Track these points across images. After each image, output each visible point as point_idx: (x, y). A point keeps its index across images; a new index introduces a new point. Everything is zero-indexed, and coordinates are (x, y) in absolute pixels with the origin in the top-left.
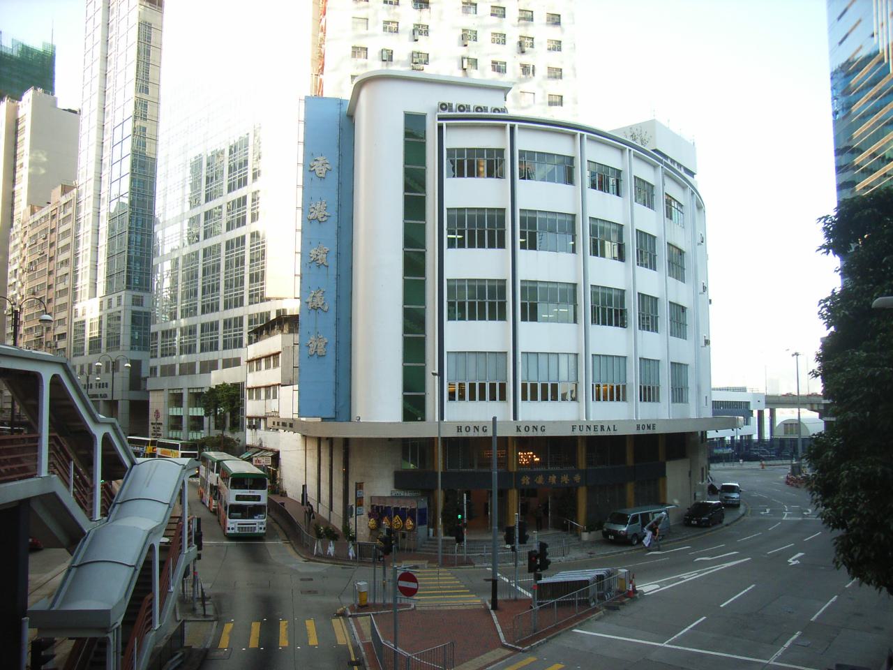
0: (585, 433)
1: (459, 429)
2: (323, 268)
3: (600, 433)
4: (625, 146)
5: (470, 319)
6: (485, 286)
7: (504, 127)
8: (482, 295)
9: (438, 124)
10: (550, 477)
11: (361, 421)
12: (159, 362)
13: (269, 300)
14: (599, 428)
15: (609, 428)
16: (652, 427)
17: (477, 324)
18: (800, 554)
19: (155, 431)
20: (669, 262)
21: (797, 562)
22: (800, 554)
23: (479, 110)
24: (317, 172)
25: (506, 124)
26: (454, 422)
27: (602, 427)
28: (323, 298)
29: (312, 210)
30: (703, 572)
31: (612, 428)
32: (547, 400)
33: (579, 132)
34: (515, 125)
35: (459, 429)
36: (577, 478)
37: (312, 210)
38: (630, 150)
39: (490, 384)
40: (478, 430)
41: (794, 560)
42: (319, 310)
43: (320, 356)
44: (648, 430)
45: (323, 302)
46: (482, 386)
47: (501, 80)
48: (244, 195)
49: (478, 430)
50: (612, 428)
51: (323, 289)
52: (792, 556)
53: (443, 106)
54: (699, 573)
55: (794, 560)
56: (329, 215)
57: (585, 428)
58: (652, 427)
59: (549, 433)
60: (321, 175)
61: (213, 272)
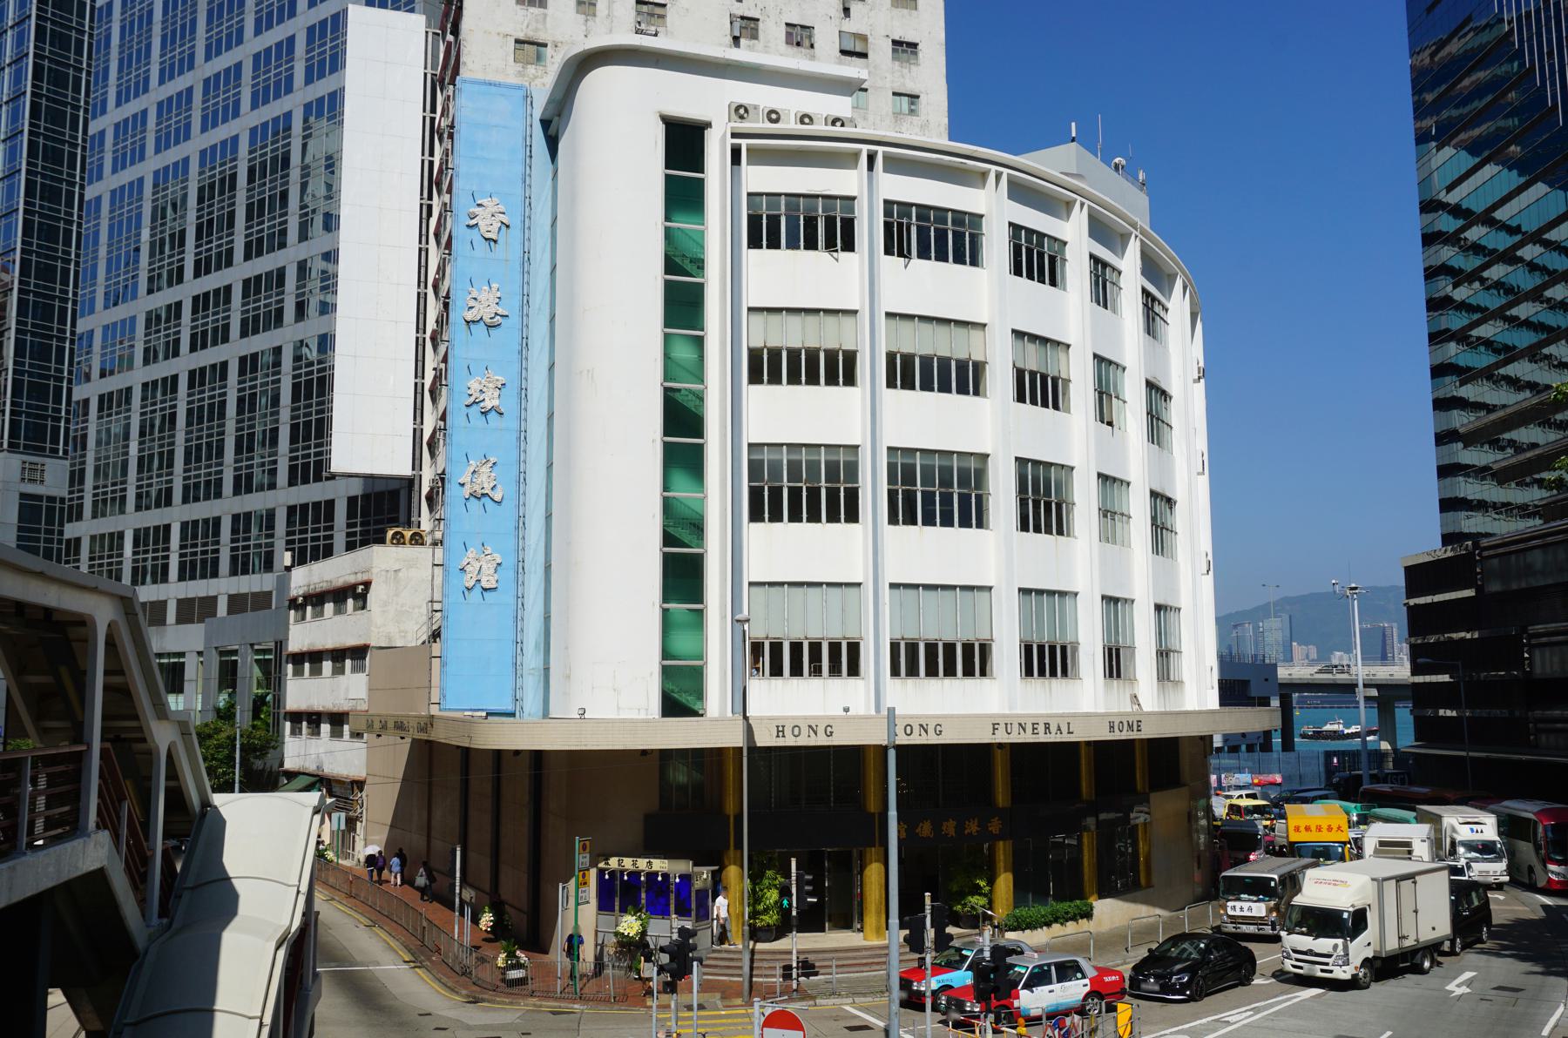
0: (1017, 737)
1: (780, 731)
2: (492, 415)
3: (1042, 738)
4: (1075, 196)
5: (771, 520)
6: (819, 462)
7: (856, 155)
8: (946, 482)
9: (732, 145)
10: (944, 824)
11: (586, 716)
12: (174, 590)
13: (333, 477)
14: (1041, 728)
15: (1059, 729)
16: (1135, 728)
17: (804, 529)
18: (1468, 975)
19: (254, 727)
20: (1148, 414)
21: (1464, 990)
22: (1468, 975)
23: (807, 120)
24: (483, 228)
25: (861, 150)
26: (771, 719)
27: (1047, 727)
28: (493, 474)
29: (472, 303)
30: (1272, 1006)
31: (1064, 729)
32: (801, 674)
33: (994, 168)
34: (876, 152)
35: (780, 731)
36: (995, 826)
37: (472, 303)
38: (1082, 205)
39: (830, 643)
40: (926, 732)
41: (1458, 986)
42: (486, 500)
43: (485, 590)
44: (1131, 733)
45: (492, 485)
46: (815, 648)
47: (852, 70)
48: (249, 263)
49: (926, 732)
50: (1064, 729)
51: (493, 460)
52: (1455, 978)
53: (741, 111)
54: (1257, 1011)
55: (1458, 986)
56: (505, 313)
57: (1016, 727)
58: (1135, 728)
59: (950, 737)
60: (488, 235)
61: (201, 408)
